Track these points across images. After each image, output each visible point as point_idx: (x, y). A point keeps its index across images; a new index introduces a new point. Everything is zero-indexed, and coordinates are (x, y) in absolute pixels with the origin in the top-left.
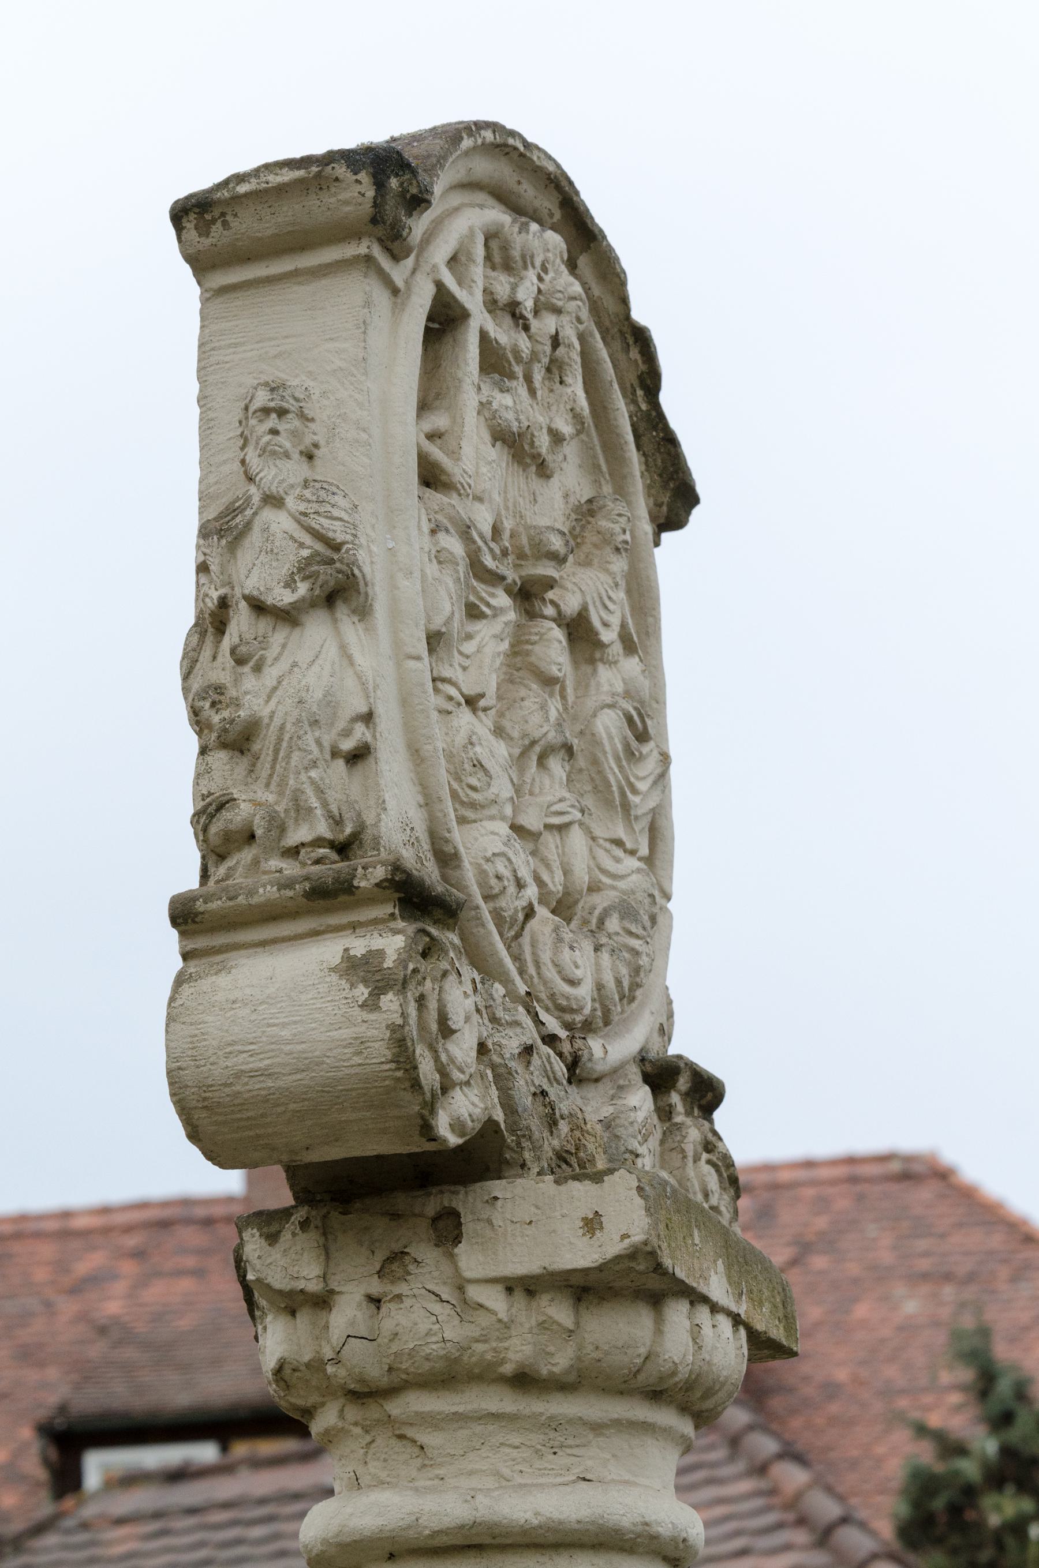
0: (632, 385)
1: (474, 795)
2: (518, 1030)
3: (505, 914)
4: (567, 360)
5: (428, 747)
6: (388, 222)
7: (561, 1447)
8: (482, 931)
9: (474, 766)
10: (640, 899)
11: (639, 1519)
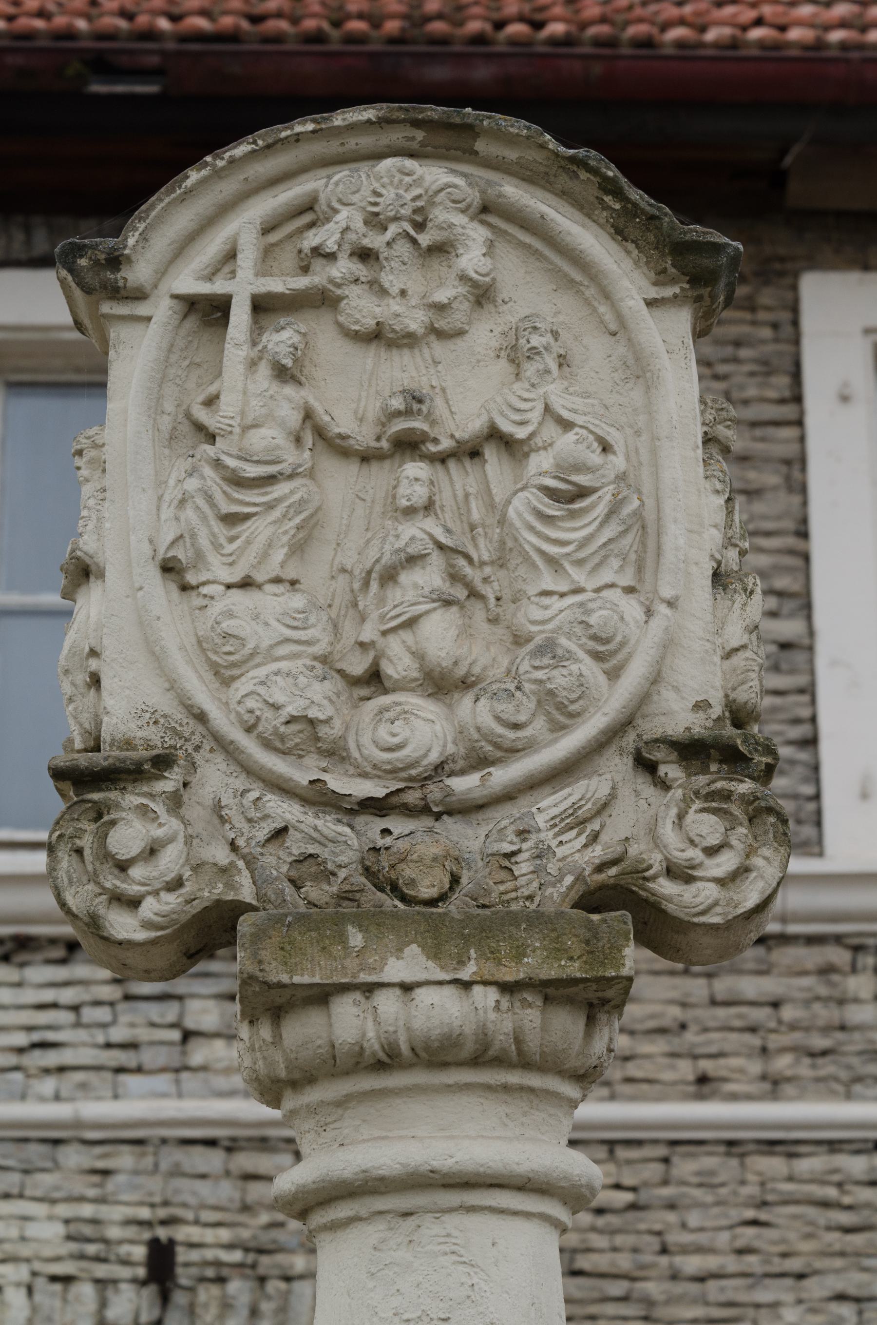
0: (597, 198)
1: (231, 658)
2: (270, 820)
3: (266, 735)
4: (453, 238)
5: (158, 648)
6: (98, 288)
7: (326, 1125)
8: (245, 756)
9: (224, 637)
10: (567, 630)
11: (358, 1169)
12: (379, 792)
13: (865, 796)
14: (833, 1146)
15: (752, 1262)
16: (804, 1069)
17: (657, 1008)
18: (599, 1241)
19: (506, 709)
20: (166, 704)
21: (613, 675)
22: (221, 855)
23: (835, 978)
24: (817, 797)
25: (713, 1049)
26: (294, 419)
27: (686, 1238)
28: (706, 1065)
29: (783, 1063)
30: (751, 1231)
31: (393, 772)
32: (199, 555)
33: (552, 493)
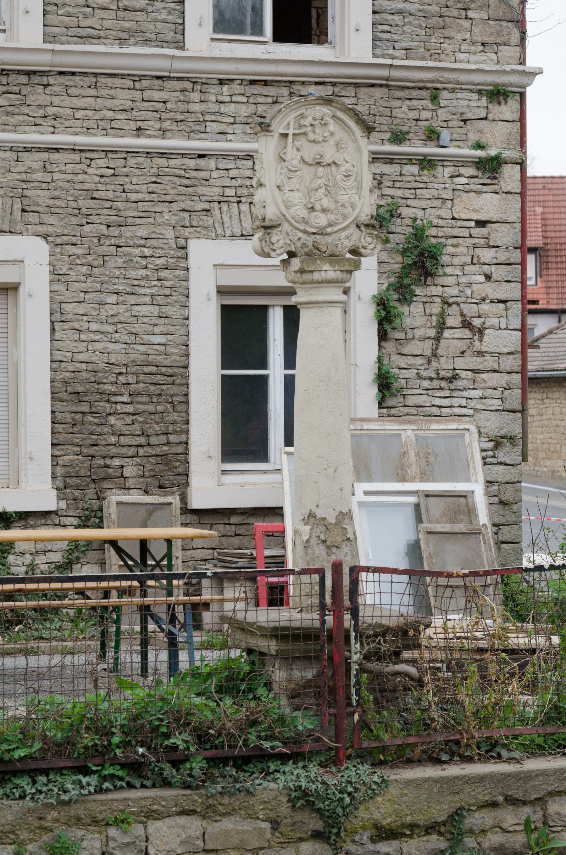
12: (315, 231)
13: (200, 25)
14: (183, 156)
15: (154, 197)
16: (174, 127)
17: (124, 102)
18: (102, 187)
19: (337, 217)
20: (278, 213)
21: (353, 210)
22: (288, 242)
23: (186, 93)
24: (183, 23)
25: (143, 118)
26: (299, 158)
27: (132, 187)
28: (139, 124)
29: (167, 124)
30: (154, 185)
31: (317, 228)
32: (283, 185)
33: (345, 176)
